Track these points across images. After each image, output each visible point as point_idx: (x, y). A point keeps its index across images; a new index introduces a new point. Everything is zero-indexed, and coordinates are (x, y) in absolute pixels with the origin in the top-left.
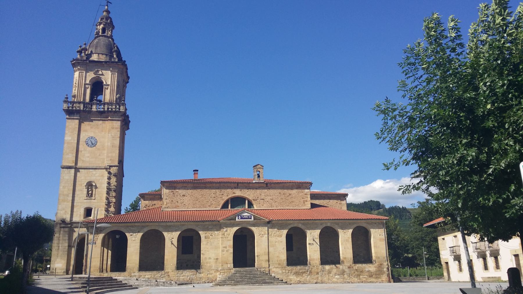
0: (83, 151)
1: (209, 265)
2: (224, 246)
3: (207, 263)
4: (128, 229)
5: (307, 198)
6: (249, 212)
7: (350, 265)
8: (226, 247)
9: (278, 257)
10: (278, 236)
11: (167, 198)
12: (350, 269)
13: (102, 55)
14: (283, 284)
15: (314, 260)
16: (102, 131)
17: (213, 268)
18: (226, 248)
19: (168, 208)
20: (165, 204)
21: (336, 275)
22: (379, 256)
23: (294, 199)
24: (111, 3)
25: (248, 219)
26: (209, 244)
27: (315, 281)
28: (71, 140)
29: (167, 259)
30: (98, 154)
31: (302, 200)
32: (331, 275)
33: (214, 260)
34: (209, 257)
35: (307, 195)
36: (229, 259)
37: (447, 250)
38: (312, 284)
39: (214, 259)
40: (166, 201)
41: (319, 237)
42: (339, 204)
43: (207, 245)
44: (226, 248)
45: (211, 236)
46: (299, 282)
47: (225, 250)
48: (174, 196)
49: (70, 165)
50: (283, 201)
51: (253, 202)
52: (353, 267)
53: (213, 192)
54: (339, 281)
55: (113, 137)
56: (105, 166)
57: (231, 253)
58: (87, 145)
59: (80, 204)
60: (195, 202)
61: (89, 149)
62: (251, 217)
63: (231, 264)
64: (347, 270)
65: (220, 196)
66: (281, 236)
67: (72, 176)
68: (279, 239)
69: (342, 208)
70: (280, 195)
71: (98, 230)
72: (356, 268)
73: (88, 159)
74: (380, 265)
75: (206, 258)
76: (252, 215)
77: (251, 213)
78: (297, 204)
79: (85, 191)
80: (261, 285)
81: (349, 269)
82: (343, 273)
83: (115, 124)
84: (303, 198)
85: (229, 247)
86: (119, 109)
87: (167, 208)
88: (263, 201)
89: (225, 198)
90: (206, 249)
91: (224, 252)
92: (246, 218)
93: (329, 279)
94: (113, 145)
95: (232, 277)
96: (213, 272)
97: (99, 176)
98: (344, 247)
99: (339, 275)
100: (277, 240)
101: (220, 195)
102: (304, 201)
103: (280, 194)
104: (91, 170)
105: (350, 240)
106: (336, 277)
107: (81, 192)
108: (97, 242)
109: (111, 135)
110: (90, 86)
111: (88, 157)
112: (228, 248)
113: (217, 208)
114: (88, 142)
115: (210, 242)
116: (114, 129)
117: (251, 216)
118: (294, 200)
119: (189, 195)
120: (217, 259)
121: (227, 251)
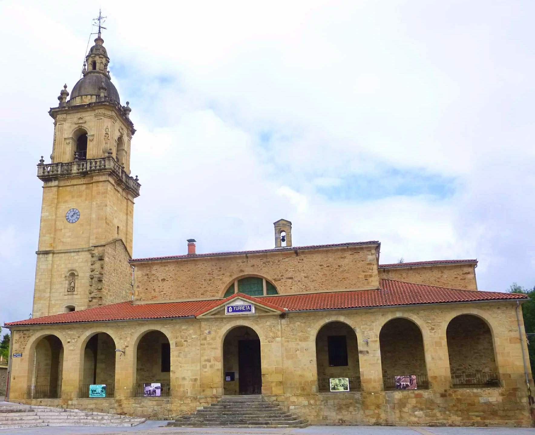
1: (182, 389)
3: (180, 386)
4: (64, 333)
5: (370, 271)
6: (245, 299)
7: (446, 391)
8: (209, 361)
9: (300, 376)
10: (300, 340)
11: (140, 284)
12: (445, 398)
13: (85, 96)
14: (286, 427)
15: (369, 381)
16: (86, 200)
17: (189, 394)
19: (140, 300)
20: (137, 294)
21: (416, 411)
22: (510, 373)
23: (346, 274)
24: (105, 28)
25: (246, 311)
26: (182, 355)
27: (374, 420)
28: (48, 216)
31: (362, 275)
32: (406, 410)
33: (191, 382)
34: (183, 376)
35: (372, 266)
38: (366, 427)
39: (192, 380)
40: (138, 289)
41: (378, 339)
42: (461, 279)
43: (179, 356)
45: (185, 341)
46: (342, 423)
47: (208, 365)
48: (149, 282)
50: (327, 278)
51: (275, 284)
52: (450, 395)
53: (208, 272)
54: (421, 421)
55: (99, 206)
56: (88, 248)
57: (218, 370)
59: (59, 302)
60: (180, 289)
61: (70, 225)
62: (250, 308)
63: (217, 389)
64: (439, 401)
65: (218, 277)
66: (305, 339)
68: (303, 344)
69: (466, 286)
70: (322, 269)
71: (25, 336)
72: (459, 397)
73: (68, 240)
74: (511, 392)
75: (177, 378)
76: (252, 304)
77: (234, 299)
78: (354, 282)
80: (245, 427)
81: (442, 399)
82: (430, 405)
83: (100, 188)
84: (364, 272)
85: (214, 360)
86: (105, 166)
88: (290, 280)
89: (228, 280)
92: (242, 311)
93: (401, 417)
95: (206, 411)
96: (189, 401)
97: (82, 262)
98: (431, 355)
99: (422, 409)
100: (299, 347)
101: (219, 275)
102: (366, 276)
103: (322, 267)
104: (73, 254)
105: (444, 342)
106: (416, 413)
107: (61, 285)
109: (97, 204)
111: (69, 237)
112: (212, 360)
115: (184, 351)
117: (250, 306)
118: (346, 275)
120: (196, 380)
121: (211, 366)
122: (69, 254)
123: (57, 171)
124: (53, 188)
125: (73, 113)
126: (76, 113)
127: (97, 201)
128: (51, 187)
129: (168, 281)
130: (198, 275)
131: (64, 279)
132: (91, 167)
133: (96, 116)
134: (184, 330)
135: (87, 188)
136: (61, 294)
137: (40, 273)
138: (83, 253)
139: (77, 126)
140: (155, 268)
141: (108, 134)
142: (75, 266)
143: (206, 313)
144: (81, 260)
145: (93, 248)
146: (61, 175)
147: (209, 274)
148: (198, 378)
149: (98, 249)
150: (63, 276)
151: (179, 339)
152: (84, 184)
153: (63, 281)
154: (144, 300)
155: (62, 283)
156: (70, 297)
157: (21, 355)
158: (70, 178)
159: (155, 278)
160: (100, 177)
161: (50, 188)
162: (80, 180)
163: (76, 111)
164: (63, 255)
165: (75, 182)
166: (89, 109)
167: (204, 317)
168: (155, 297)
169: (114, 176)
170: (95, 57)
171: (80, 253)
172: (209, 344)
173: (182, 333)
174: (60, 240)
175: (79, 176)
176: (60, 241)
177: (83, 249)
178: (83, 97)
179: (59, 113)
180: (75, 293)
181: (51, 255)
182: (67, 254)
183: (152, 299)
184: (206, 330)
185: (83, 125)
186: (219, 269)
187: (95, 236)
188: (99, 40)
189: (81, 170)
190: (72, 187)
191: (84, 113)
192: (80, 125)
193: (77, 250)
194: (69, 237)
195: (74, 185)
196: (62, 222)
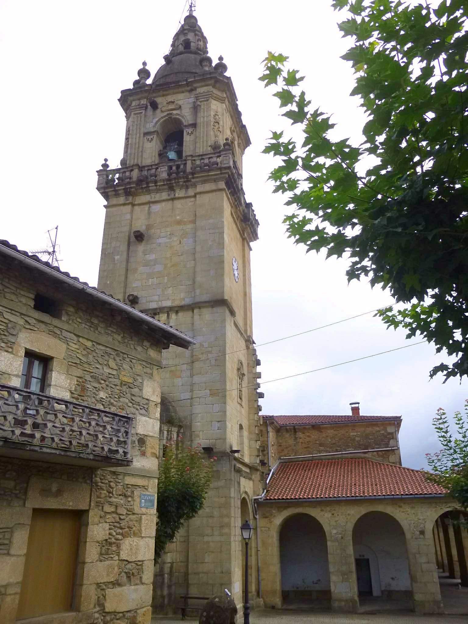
24: (444, 383)
141: (219, 124)
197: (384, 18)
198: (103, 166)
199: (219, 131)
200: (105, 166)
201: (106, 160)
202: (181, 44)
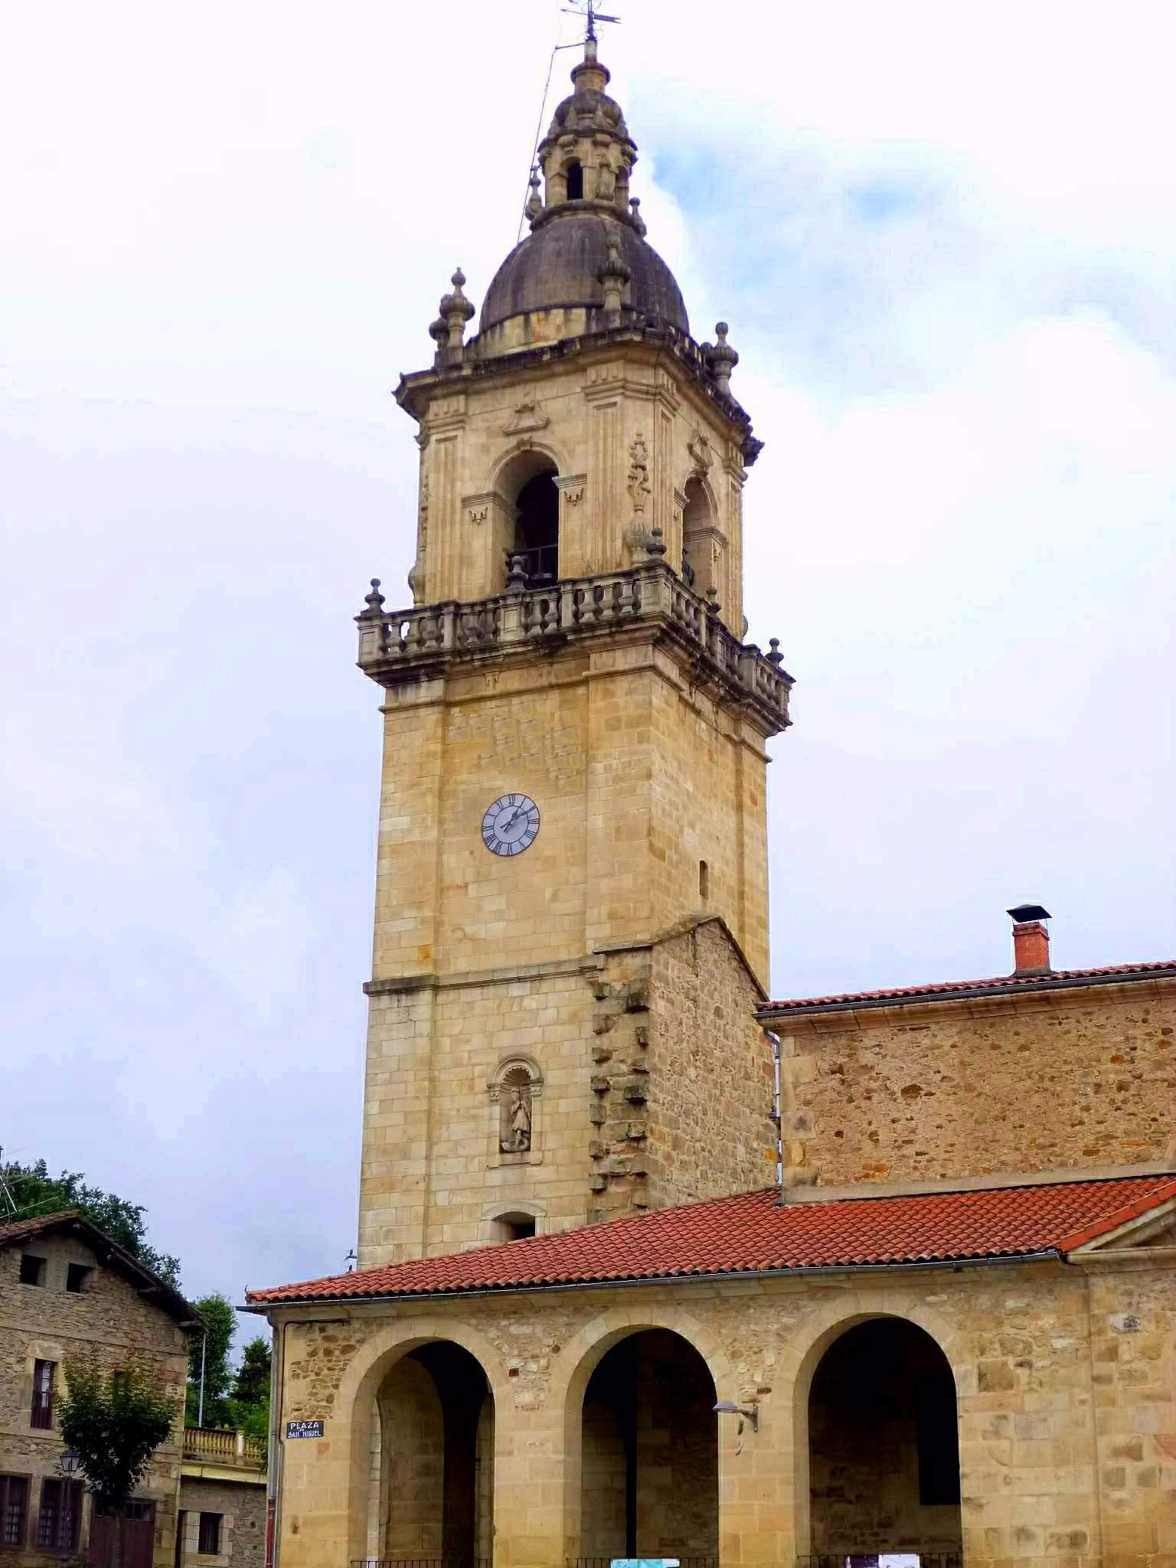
0: (471, 887)
2: (1121, 1440)
8: (1133, 1453)
13: (542, 315)
18: (1139, 1458)
19: (814, 1182)
24: (611, 19)
29: (735, 1539)
30: (548, 894)
33: (1053, 1550)
36: (1159, 1540)
37: (1123, 1469)
40: (802, 1134)
43: (997, 1434)
44: (1139, 1458)
45: (1021, 1365)
47: (1128, 1471)
48: (851, 1100)
49: (407, 974)
56: (580, 960)
58: (492, 847)
67: (421, 1036)
71: (332, 1346)
73: (497, 928)
75: (993, 1532)
79: (492, 1119)
86: (636, 605)
87: (808, 1187)
90: (994, 1467)
91: (1121, 1484)
94: (618, 830)
97: (558, 1022)
104: (515, 990)
107: (472, 1125)
108: (327, 1423)
110: (490, 505)
112: (1146, 1452)
113: (1145, 1160)
114: (492, 827)
115: (1021, 1411)
116: (618, 728)
119: (945, 1085)
120: (1076, 1540)
121: (1145, 1479)
122: (501, 990)
123: (440, 638)
124: (423, 712)
125: (496, 388)
126: (504, 387)
127: (607, 756)
128: (416, 706)
129: (930, 1094)
130: (1066, 1068)
131: (485, 1097)
132: (577, 615)
133: (589, 394)
134: (1013, 1313)
135: (562, 704)
136: (476, 1161)
137: (386, 1076)
138: (560, 984)
139: (513, 441)
140: (870, 1037)
141: (644, 468)
142: (528, 1040)
143: (1108, 1237)
144: (551, 1013)
145: (600, 961)
146: (456, 652)
147: (1114, 1060)
148: (1088, 1529)
149: (620, 964)
150: (481, 1085)
151: (994, 1357)
152: (552, 687)
153: (481, 1106)
154: (829, 1182)
155: (475, 1117)
156: (511, 1174)
157: (321, 1430)
158: (494, 664)
159: (874, 1085)
160: (619, 654)
161: (410, 713)
162: (534, 672)
163: (505, 380)
164: (476, 993)
165: (511, 680)
166: (559, 368)
167: (1102, 1255)
168: (879, 1169)
169: (676, 648)
170: (575, 143)
171: (545, 986)
172: (1130, 1376)
173: (1008, 1330)
174: (461, 929)
175: (529, 656)
176: (459, 934)
177: (559, 964)
178: (534, 317)
179: (438, 392)
180: (532, 1156)
181: (426, 996)
182: (491, 990)
183: (867, 1176)
184: (1114, 1312)
185: (537, 437)
186: (1162, 1037)
187: (605, 910)
188: (590, 72)
189: (537, 630)
190: (505, 701)
191: (539, 385)
192: (526, 436)
193: (534, 972)
194: (499, 915)
195: (508, 695)
196: (467, 853)
197: (684, 643)
198: (368, 600)
199: (644, 489)
200: (376, 599)
201: (375, 583)
202: (559, 174)
